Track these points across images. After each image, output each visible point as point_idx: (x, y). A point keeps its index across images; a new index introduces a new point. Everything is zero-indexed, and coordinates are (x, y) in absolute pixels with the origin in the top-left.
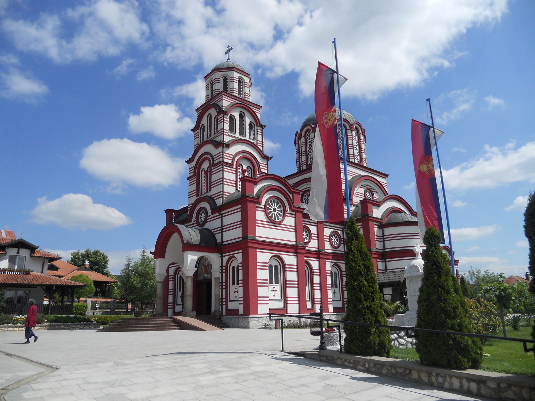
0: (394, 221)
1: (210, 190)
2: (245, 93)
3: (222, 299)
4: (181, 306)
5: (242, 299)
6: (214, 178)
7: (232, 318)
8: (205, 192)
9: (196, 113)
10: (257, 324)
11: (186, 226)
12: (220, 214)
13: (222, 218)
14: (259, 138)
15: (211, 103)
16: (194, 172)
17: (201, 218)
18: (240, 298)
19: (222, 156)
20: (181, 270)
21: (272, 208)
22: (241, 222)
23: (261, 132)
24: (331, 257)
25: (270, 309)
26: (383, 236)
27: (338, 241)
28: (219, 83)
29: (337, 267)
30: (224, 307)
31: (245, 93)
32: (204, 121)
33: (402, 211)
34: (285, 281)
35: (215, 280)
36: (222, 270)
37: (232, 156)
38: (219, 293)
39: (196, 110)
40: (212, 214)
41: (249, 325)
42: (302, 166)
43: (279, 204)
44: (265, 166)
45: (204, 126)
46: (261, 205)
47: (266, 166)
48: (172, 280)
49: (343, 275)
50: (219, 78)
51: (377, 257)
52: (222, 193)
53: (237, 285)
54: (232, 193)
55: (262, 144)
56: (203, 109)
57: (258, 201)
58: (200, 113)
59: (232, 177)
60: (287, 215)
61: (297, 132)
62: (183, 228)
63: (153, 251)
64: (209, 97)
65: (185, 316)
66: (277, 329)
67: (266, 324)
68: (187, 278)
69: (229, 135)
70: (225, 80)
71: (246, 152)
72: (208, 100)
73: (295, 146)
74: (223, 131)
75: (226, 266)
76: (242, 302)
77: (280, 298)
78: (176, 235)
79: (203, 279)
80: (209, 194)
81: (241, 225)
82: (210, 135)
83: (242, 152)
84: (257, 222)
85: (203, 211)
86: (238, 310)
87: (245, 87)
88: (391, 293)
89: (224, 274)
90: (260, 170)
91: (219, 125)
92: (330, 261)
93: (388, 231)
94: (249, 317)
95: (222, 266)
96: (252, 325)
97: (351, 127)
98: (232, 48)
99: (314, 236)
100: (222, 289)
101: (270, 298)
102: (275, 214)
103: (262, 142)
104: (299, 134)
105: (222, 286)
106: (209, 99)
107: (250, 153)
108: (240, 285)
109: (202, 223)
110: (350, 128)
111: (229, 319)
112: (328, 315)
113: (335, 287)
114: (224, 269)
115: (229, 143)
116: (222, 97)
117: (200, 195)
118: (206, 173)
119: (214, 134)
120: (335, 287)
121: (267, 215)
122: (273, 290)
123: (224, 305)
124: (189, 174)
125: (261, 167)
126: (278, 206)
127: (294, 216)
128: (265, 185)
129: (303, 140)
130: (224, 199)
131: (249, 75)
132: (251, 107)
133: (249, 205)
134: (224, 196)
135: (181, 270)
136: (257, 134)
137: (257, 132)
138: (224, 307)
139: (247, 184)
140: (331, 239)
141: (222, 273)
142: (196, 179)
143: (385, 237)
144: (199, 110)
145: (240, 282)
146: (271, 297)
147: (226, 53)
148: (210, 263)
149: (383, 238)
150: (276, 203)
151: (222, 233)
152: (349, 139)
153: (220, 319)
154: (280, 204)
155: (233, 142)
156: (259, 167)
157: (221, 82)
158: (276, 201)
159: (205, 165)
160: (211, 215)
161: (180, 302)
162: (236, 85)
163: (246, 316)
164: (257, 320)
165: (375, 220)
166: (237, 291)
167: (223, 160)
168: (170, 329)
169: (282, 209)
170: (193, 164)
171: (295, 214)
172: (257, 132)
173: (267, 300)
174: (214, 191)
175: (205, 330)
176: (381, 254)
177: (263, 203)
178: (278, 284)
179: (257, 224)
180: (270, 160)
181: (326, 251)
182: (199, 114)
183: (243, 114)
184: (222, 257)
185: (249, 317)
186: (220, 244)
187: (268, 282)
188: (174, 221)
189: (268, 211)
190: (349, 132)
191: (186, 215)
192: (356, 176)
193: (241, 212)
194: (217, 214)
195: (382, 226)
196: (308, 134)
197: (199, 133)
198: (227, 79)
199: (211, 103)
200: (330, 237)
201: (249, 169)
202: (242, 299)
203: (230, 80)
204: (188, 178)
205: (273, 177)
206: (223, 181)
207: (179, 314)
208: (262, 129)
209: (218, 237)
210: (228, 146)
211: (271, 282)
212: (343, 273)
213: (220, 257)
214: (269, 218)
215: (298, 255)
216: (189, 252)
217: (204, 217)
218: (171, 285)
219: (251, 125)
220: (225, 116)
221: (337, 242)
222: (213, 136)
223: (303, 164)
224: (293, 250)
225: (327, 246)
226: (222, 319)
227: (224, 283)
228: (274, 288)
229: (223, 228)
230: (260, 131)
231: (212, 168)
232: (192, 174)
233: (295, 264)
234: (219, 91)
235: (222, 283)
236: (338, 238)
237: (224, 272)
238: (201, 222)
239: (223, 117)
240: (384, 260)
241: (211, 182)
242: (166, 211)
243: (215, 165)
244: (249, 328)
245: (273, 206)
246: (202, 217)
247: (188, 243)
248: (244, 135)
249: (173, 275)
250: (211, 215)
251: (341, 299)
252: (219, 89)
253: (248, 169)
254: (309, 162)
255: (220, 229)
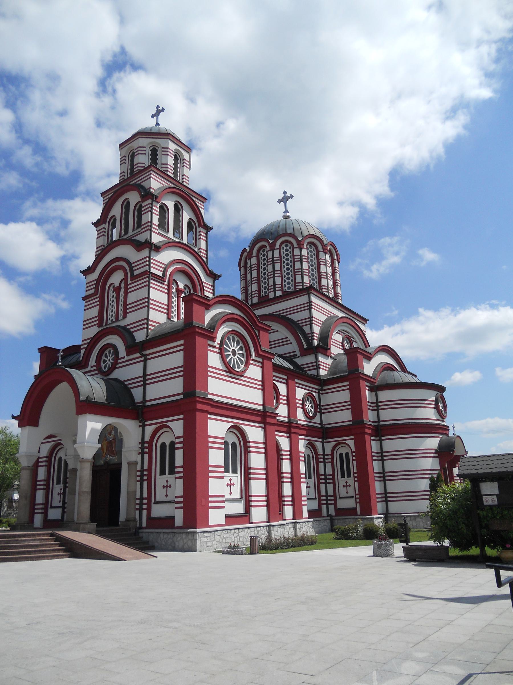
0: (390, 381)
1: (124, 317)
2: (184, 175)
3: (141, 498)
4: (60, 510)
5: (181, 500)
6: (132, 298)
7: (160, 533)
8: (114, 320)
9: (102, 199)
10: (209, 544)
11: (84, 373)
12: (143, 355)
13: (145, 361)
14: (203, 244)
15: (132, 183)
16: (96, 288)
17: (105, 361)
18: (177, 497)
19: (147, 263)
20: (62, 448)
21: (230, 349)
22: (182, 369)
23: (205, 237)
24: (304, 432)
25: (228, 517)
26: (377, 402)
27: (312, 409)
28: (145, 154)
29: (311, 448)
30: (145, 512)
31: (184, 175)
32: (116, 211)
33: (395, 369)
34: (247, 468)
35: (129, 465)
36: (142, 448)
37: (164, 266)
38: (136, 489)
39: (103, 194)
40: (128, 354)
41: (195, 545)
42: (252, 299)
43: (241, 345)
44: (210, 287)
45: (115, 219)
46: (215, 342)
47: (212, 288)
48: (45, 466)
49: (320, 460)
50: (145, 147)
51: (370, 433)
52: (146, 321)
53: (169, 474)
54: (162, 323)
55: (207, 254)
56: (115, 192)
57: (211, 335)
58: (110, 198)
59: (163, 298)
60: (252, 362)
61: (244, 250)
62: (78, 374)
63: (17, 413)
64: (126, 175)
65: (77, 530)
66: (255, 554)
67: (233, 545)
68: (84, 462)
69: (159, 234)
70: (154, 153)
71: (185, 262)
72: (123, 178)
73: (240, 270)
74: (151, 226)
75: (151, 442)
76: (181, 505)
77: (239, 497)
78: (64, 387)
79: (105, 464)
80: (122, 323)
81: (182, 373)
82: (126, 232)
83: (177, 261)
84: (209, 369)
85: (110, 352)
86: (172, 518)
87: (184, 166)
88: (497, 492)
89: (146, 456)
90: (203, 293)
91: (143, 216)
92: (303, 437)
93: (384, 395)
94: (195, 533)
95: (143, 442)
96: (201, 545)
97: (324, 248)
98: (163, 110)
99: (283, 399)
100: (142, 481)
101: (226, 497)
102: (234, 359)
103: (207, 251)
104: (248, 253)
105: (142, 476)
106: (126, 178)
107: (190, 265)
108: (177, 475)
109: (107, 369)
110: (323, 249)
111: (155, 534)
112: (302, 522)
113: (308, 479)
114: (146, 448)
115: (161, 244)
116: (151, 174)
117: (104, 324)
118: (117, 290)
119: (133, 230)
120: (308, 479)
121: (223, 359)
122: (229, 483)
123: (145, 509)
124: (86, 291)
125: (205, 288)
126: (239, 347)
127: (260, 365)
128: (221, 313)
129: (254, 260)
130: (149, 331)
131: (191, 150)
132: (194, 199)
133: (199, 340)
134: (150, 327)
135: (62, 448)
136: (200, 238)
137: (200, 235)
138: (145, 512)
139: (196, 307)
140: (304, 405)
141: (142, 453)
142: (98, 299)
143: (380, 404)
144: (106, 195)
145: (177, 470)
146: (228, 496)
147: (153, 116)
148: (121, 436)
149: (377, 406)
150: (236, 343)
151: (144, 386)
152: (322, 278)
153: (136, 534)
154: (241, 344)
155: (165, 244)
156: (202, 288)
157: (147, 154)
158: (236, 339)
159: (116, 278)
160: (126, 357)
161: (57, 500)
162: (171, 161)
163: (189, 530)
164: (209, 537)
165: (367, 379)
166: (168, 485)
167: (150, 269)
168: (53, 557)
169: (243, 352)
170: (95, 276)
171: (262, 361)
172: (200, 235)
173: (223, 500)
174: (131, 318)
175: (125, 560)
176: (374, 428)
177: (218, 340)
178: (237, 473)
179: (209, 373)
180: (218, 279)
181: (299, 422)
182: (107, 200)
183: (179, 206)
184: (143, 427)
185: (195, 533)
186: (142, 404)
187: (223, 470)
188: (60, 363)
189: (226, 354)
190: (322, 255)
191: (78, 356)
192: (332, 317)
193: (182, 353)
194: (138, 355)
195: (375, 389)
196: (261, 253)
197: (105, 229)
198: (157, 151)
199: (132, 183)
200: (303, 401)
201: (187, 289)
202: (181, 500)
203: (163, 151)
204: (84, 298)
205: (232, 300)
206: (148, 302)
207: (59, 524)
208: (207, 233)
209: (137, 394)
210: (157, 248)
211: (227, 471)
212: (319, 457)
213: (140, 426)
214: (226, 364)
215: (267, 426)
216: (89, 416)
217: (111, 361)
218: (42, 473)
219: (189, 223)
220: (154, 203)
221: (312, 410)
222: (130, 232)
223: (253, 296)
224: (259, 419)
225: (300, 414)
226: (141, 535)
227: (146, 470)
228: (230, 480)
229: (148, 377)
230: (204, 235)
231: (129, 282)
232: (93, 291)
233: (262, 441)
234: (144, 167)
235: (142, 470)
236: (312, 404)
237: (146, 453)
238: (105, 368)
239: (152, 204)
240: (378, 438)
241: (125, 304)
242: (41, 350)
243: (134, 278)
244: (195, 551)
245: (232, 347)
246: (108, 360)
247: (89, 399)
248: (181, 237)
249: (46, 457)
250: (126, 357)
251: (317, 498)
252: (144, 164)
253: (185, 288)
254: (263, 293)
255: (142, 379)
